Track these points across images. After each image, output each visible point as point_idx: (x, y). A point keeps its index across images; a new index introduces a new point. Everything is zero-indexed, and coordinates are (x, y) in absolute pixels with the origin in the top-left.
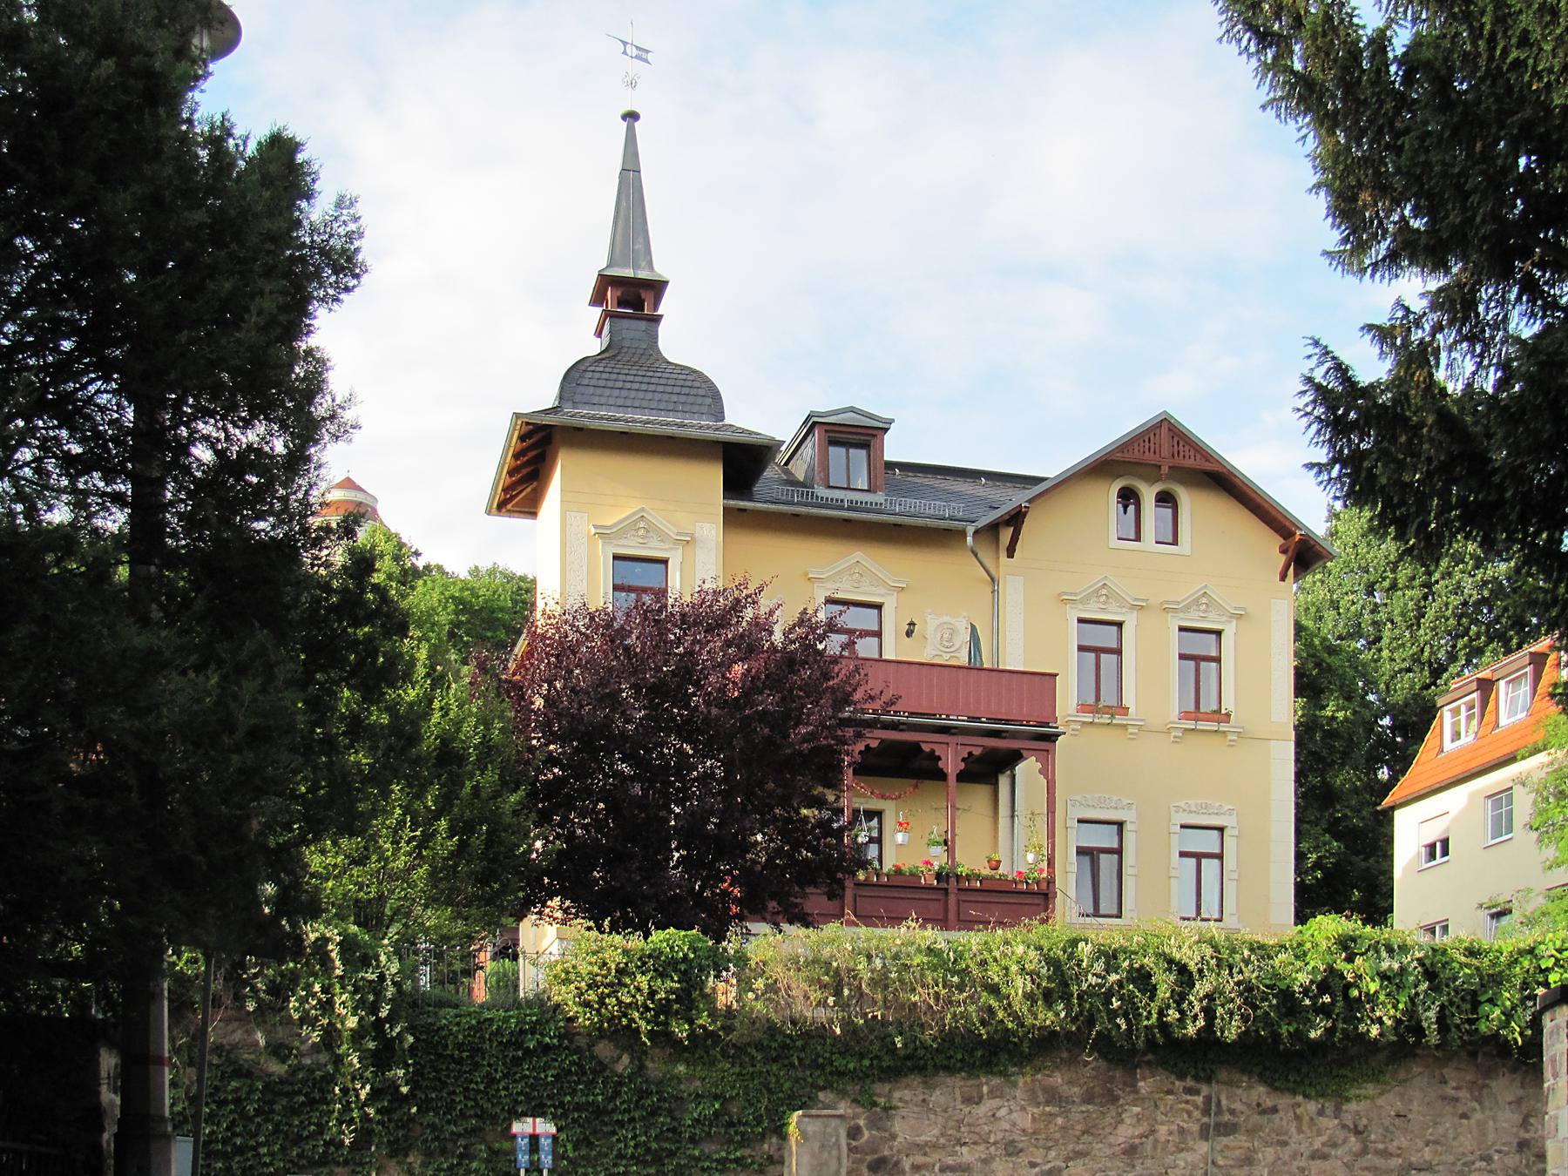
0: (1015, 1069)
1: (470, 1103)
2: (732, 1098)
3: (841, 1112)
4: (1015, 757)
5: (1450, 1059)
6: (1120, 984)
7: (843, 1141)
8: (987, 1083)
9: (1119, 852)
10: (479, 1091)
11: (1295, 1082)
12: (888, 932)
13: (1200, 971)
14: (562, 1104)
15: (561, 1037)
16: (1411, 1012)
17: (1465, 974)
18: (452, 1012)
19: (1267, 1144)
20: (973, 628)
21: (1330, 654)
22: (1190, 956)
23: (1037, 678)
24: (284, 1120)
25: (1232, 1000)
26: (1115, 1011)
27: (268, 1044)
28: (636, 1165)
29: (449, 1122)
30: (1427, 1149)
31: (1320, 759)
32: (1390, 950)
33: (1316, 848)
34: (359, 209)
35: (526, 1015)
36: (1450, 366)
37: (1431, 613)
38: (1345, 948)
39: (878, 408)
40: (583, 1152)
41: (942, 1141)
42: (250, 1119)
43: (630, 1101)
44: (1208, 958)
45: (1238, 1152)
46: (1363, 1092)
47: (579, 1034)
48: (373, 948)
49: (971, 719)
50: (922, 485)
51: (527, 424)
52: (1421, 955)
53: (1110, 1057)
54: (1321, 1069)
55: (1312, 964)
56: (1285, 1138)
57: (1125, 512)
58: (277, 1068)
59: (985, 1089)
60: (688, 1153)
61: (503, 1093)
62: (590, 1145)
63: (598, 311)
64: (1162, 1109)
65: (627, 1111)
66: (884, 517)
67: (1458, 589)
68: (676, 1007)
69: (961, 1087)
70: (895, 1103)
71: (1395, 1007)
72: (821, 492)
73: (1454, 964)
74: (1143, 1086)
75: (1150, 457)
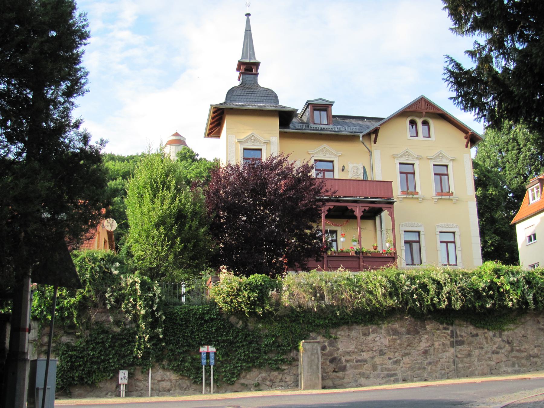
0: (381, 322)
1: (185, 341)
2: (279, 336)
3: (318, 340)
4: (380, 211)
5: (540, 314)
6: (416, 289)
7: (319, 351)
8: (371, 328)
9: (419, 242)
10: (188, 336)
11: (483, 324)
12: (332, 273)
13: (445, 283)
14: (218, 340)
15: (217, 315)
16: (523, 297)
17: (541, 282)
18: (179, 307)
19: (476, 348)
20: (364, 167)
21: (489, 173)
22: (440, 278)
23: (386, 183)
24: (119, 349)
25: (457, 294)
26: (415, 299)
27: (114, 321)
28: (245, 363)
29: (177, 348)
30: (536, 349)
31: (489, 208)
32: (513, 274)
33: (491, 239)
34: (88, 17)
35: (205, 307)
36: (497, 63)
37: (521, 158)
38: (497, 273)
39: (329, 98)
40: (225, 358)
41: (356, 350)
42: (107, 349)
43: (242, 338)
44: (447, 279)
45: (465, 352)
46: (509, 327)
47: (223, 314)
48: (151, 284)
49: (365, 198)
50: (345, 122)
51: (215, 108)
52: (524, 275)
53: (415, 316)
54: (493, 319)
55: (485, 279)
56: (482, 346)
57: (412, 128)
58: (117, 330)
59: (371, 330)
60: (263, 357)
61: (197, 337)
62: (228, 355)
63: (239, 72)
64: (436, 336)
65: (241, 342)
66: (333, 133)
67: (529, 150)
68: (258, 302)
69: (362, 329)
70: (338, 336)
71: (517, 295)
72: (312, 125)
73: (537, 278)
74: (428, 327)
75: (418, 110)
